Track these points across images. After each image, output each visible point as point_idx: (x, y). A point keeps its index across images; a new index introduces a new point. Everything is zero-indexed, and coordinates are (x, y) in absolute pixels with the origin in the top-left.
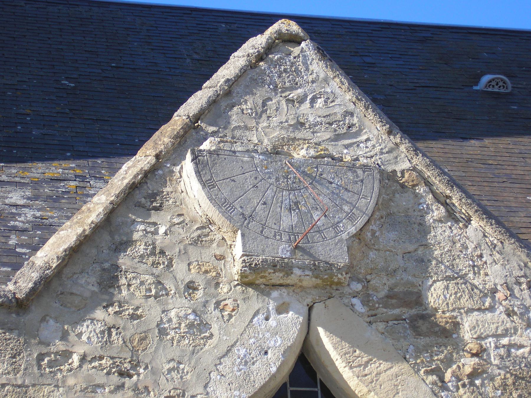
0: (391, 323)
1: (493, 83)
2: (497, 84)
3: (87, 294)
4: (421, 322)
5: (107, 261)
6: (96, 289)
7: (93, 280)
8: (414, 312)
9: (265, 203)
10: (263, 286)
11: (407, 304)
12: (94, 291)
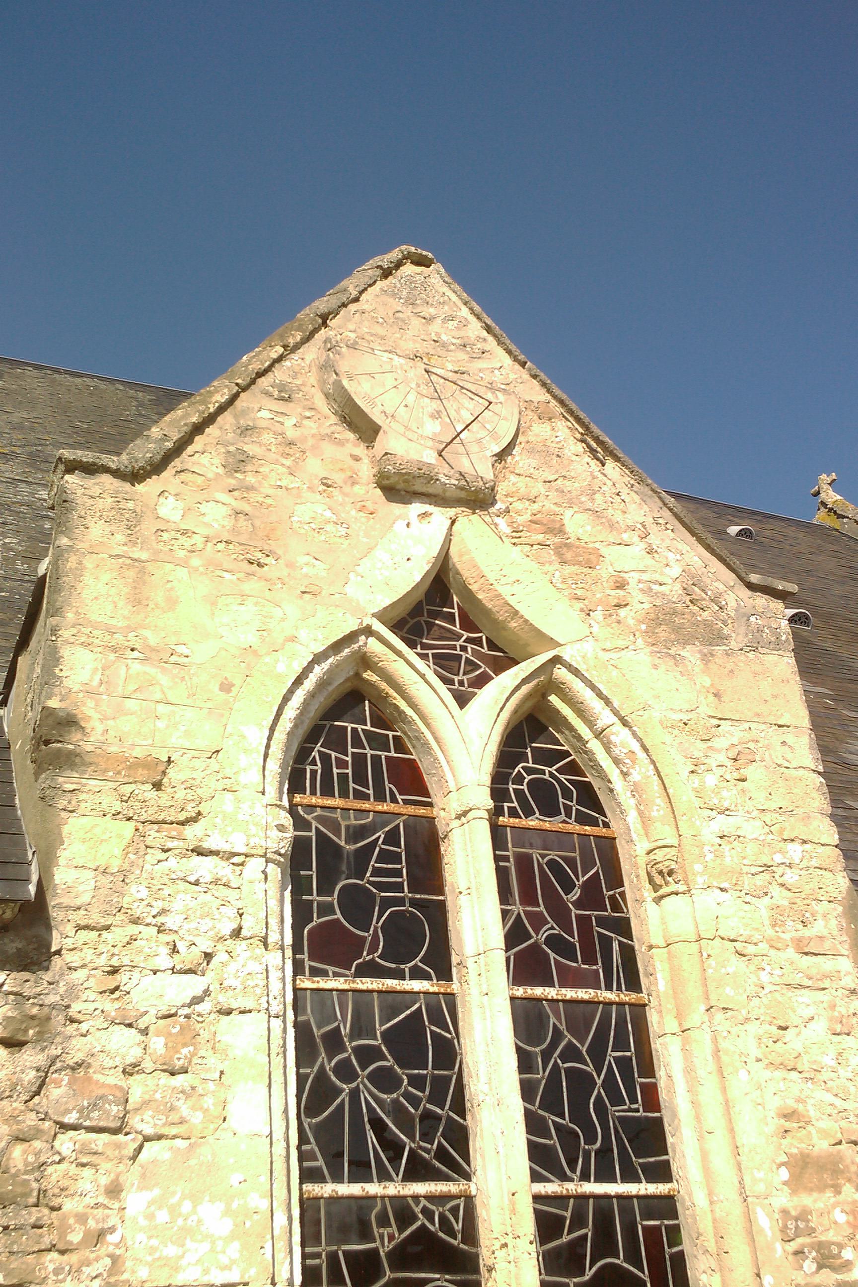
0: (535, 547)
1: (743, 533)
2: (799, 620)
3: (210, 475)
4: (565, 549)
5: (233, 444)
6: (221, 471)
7: (217, 461)
8: (557, 540)
9: (406, 406)
10: (403, 493)
11: (550, 531)
12: (218, 473)
